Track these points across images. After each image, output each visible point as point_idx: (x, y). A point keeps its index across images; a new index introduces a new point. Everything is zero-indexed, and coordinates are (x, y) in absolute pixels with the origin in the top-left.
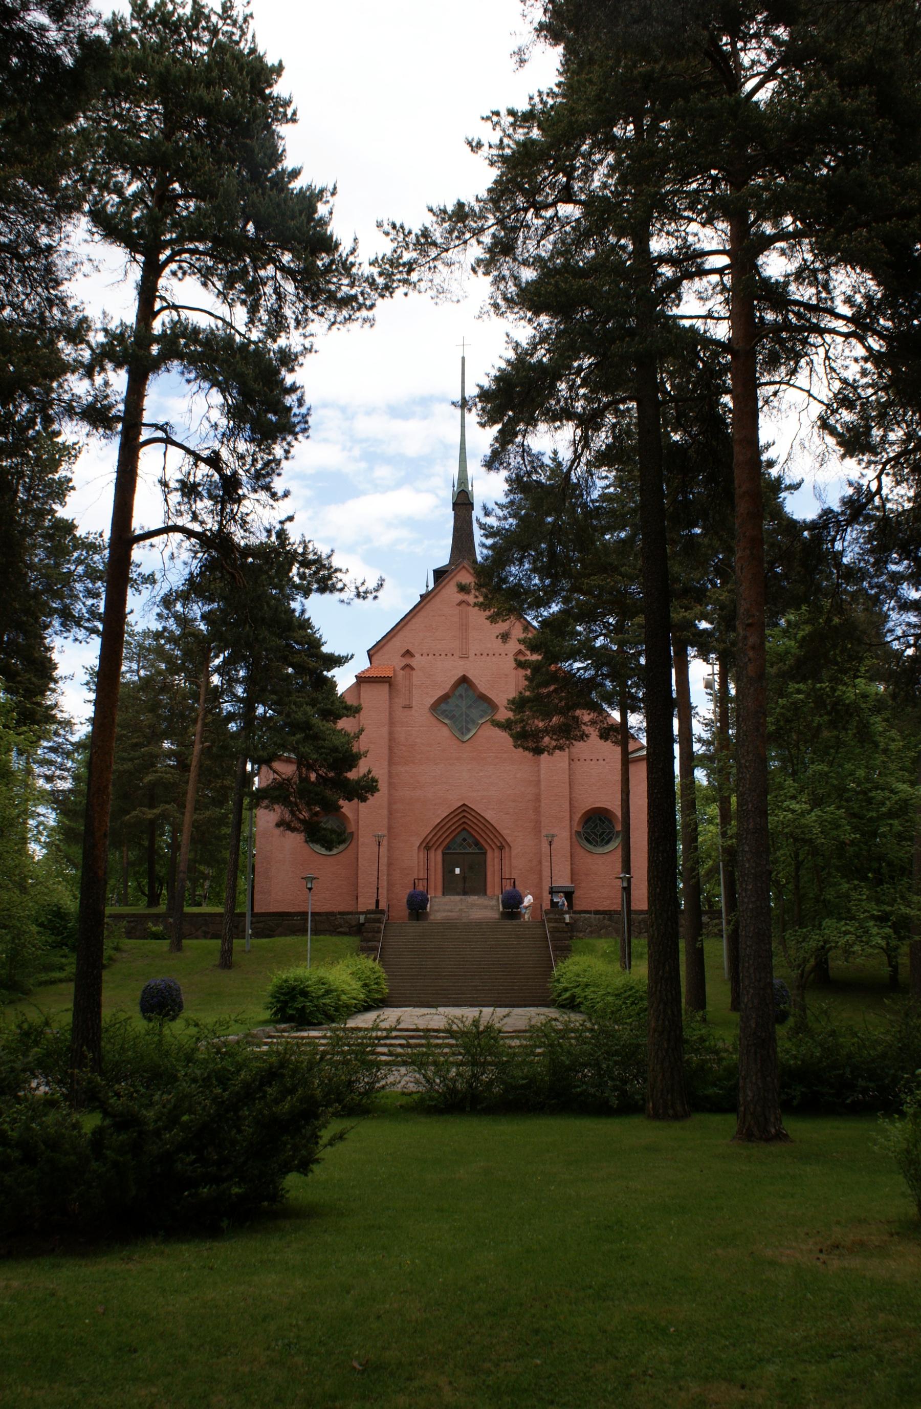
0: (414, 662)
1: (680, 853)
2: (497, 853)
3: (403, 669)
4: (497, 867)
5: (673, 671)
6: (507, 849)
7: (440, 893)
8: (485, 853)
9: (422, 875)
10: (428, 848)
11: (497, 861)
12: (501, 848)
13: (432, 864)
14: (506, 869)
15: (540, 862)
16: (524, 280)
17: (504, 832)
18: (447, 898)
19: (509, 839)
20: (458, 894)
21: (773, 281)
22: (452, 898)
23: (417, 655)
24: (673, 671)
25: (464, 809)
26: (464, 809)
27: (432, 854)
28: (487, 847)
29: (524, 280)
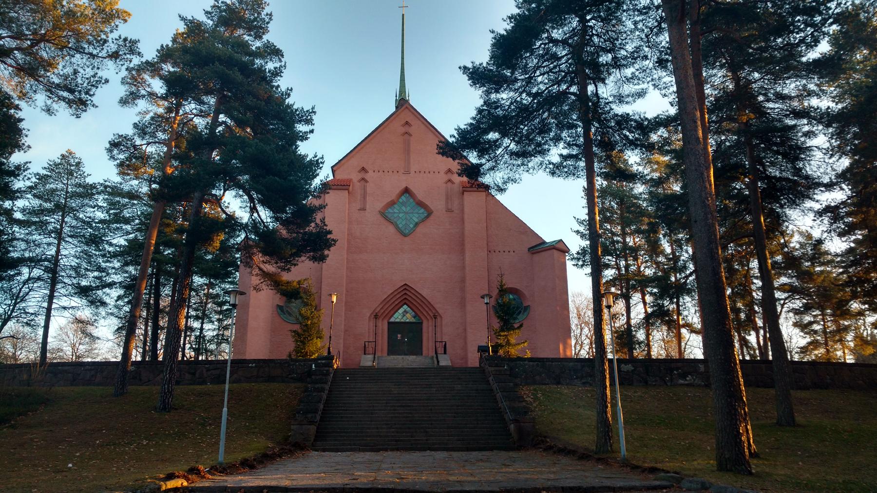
0: (368, 177)
3: (359, 181)
8: (421, 323)
10: (376, 317)
14: (438, 334)
17: (437, 306)
19: (440, 311)
23: (371, 172)
25: (406, 288)
26: (406, 288)
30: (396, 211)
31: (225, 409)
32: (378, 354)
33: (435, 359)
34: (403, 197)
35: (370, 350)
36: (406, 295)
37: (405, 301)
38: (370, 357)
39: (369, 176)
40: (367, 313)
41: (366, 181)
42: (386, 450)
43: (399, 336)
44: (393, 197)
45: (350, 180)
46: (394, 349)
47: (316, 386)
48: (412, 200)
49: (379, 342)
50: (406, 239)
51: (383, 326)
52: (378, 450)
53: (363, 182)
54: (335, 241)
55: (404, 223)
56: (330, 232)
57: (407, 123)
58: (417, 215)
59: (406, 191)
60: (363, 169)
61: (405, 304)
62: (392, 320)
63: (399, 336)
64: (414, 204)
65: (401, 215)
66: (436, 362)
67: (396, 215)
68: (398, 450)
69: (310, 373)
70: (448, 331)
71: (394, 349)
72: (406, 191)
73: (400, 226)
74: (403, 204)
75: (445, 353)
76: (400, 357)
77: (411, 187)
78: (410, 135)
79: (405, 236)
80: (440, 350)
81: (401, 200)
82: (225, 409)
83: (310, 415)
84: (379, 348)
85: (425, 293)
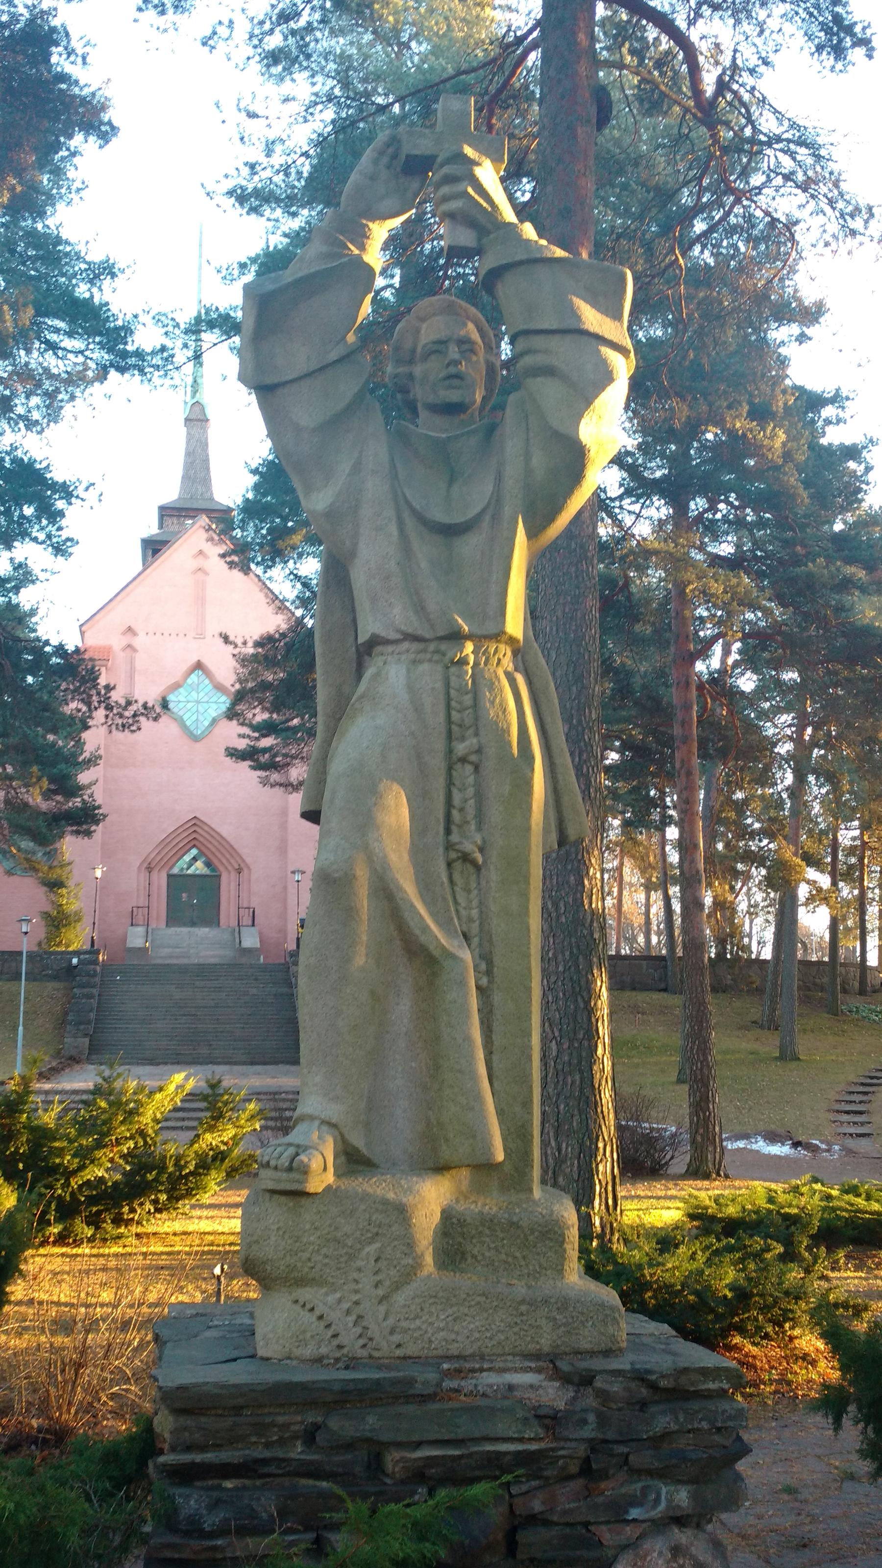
0: (137, 642)
1: (318, 1483)
2: (233, 874)
3: (124, 649)
4: (233, 893)
5: (457, 617)
6: (246, 871)
7: (163, 925)
8: (219, 876)
9: (143, 902)
10: (150, 869)
11: (233, 886)
12: (239, 871)
13: (154, 888)
14: (244, 895)
15: (285, 888)
16: (371, 225)
17: (244, 852)
18: (173, 930)
19: (248, 860)
20: (185, 925)
21: (250, 496)
22: (178, 930)
23: (142, 634)
24: (457, 617)
25: (196, 822)
26: (196, 822)
27: (155, 874)
28: (221, 868)
29: (371, 225)
30: (181, 698)
31: (21, 1028)
32: (153, 925)
33: (237, 935)
34: (193, 676)
35: (140, 919)
36: (195, 834)
37: (193, 843)
38: (141, 930)
39: (139, 642)
40: (135, 861)
41: (135, 650)
42: (166, 1063)
43: (184, 895)
44: (177, 676)
45: (109, 649)
46: (175, 917)
47: (85, 991)
48: (207, 681)
49: (154, 905)
50: (198, 745)
51: (161, 880)
52: (158, 1064)
53: (128, 650)
54: (105, 816)
55: (194, 718)
56: (99, 807)
57: (201, 552)
58: (214, 706)
59: (199, 666)
60: (130, 629)
61: (194, 846)
62: (175, 871)
63: (184, 895)
64: (210, 687)
65: (190, 705)
66: (237, 941)
67: (181, 705)
68: (178, 1063)
69: (71, 969)
70: (259, 888)
71: (175, 917)
72: (199, 666)
73: (188, 723)
74: (196, 688)
75: (253, 925)
76: (185, 930)
77: (206, 662)
78: (206, 573)
79: (196, 739)
80: (247, 920)
81: (189, 681)
82: (21, 1028)
83: (82, 1027)
84: (154, 913)
85: (226, 831)
